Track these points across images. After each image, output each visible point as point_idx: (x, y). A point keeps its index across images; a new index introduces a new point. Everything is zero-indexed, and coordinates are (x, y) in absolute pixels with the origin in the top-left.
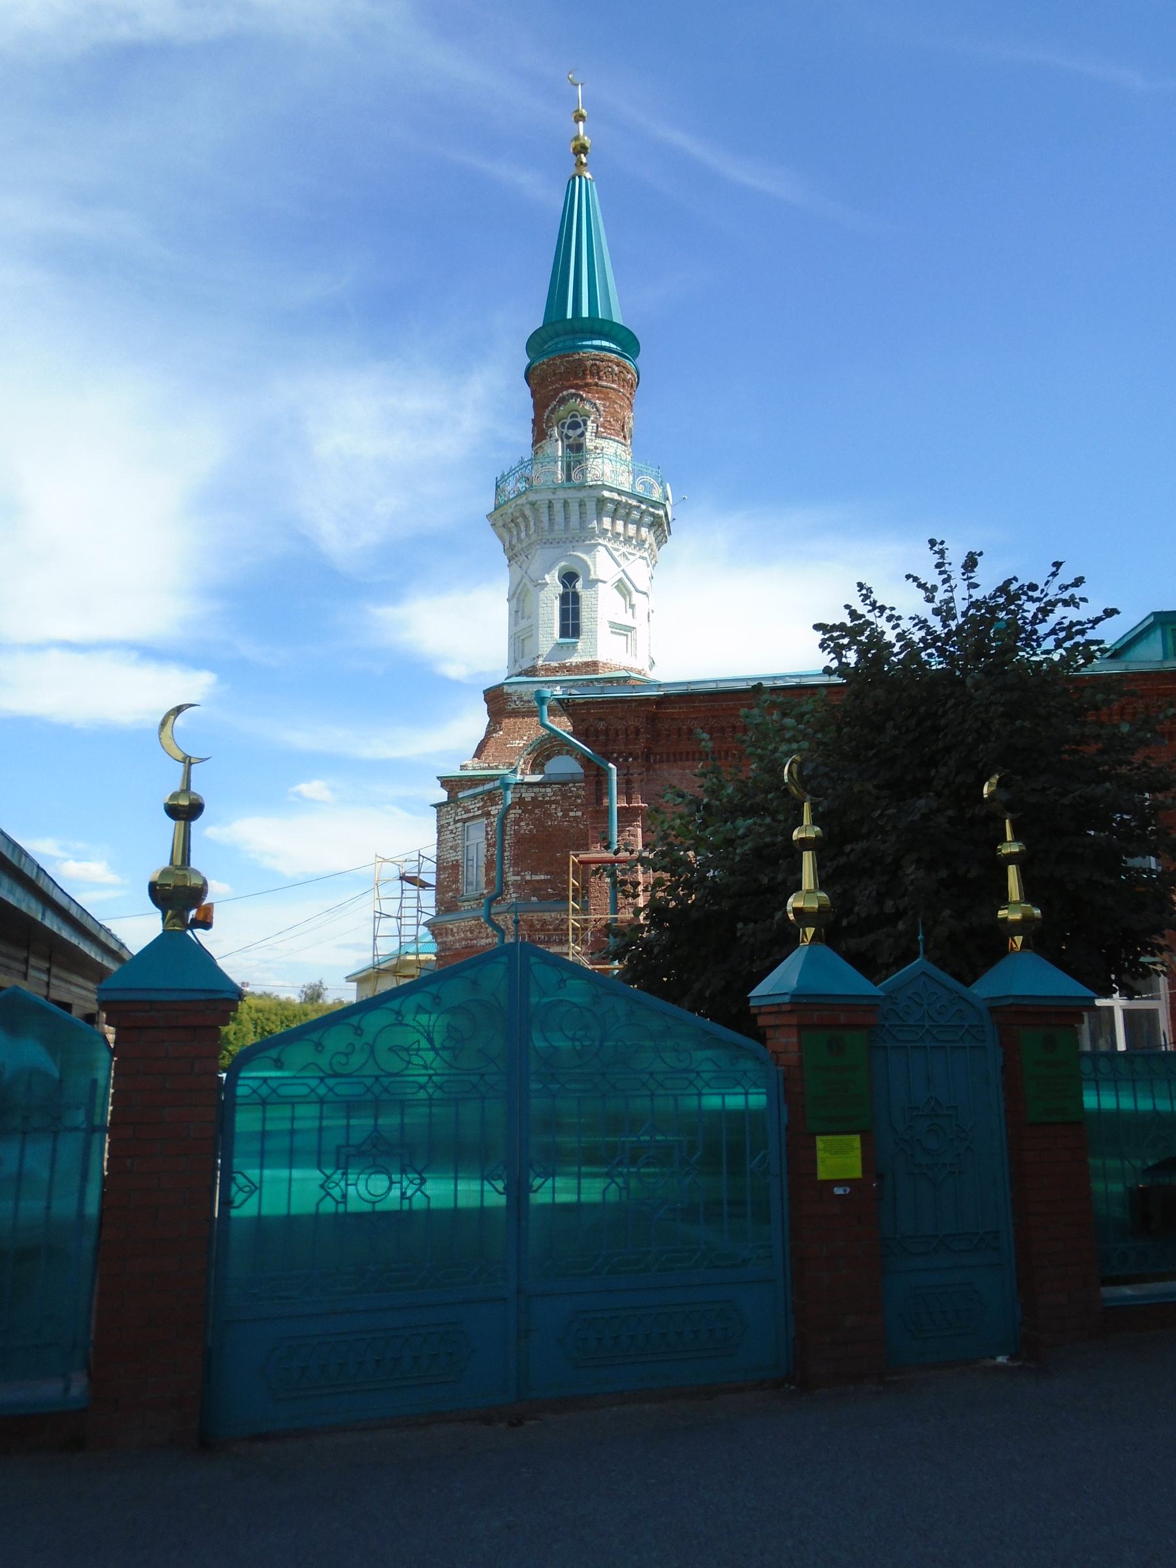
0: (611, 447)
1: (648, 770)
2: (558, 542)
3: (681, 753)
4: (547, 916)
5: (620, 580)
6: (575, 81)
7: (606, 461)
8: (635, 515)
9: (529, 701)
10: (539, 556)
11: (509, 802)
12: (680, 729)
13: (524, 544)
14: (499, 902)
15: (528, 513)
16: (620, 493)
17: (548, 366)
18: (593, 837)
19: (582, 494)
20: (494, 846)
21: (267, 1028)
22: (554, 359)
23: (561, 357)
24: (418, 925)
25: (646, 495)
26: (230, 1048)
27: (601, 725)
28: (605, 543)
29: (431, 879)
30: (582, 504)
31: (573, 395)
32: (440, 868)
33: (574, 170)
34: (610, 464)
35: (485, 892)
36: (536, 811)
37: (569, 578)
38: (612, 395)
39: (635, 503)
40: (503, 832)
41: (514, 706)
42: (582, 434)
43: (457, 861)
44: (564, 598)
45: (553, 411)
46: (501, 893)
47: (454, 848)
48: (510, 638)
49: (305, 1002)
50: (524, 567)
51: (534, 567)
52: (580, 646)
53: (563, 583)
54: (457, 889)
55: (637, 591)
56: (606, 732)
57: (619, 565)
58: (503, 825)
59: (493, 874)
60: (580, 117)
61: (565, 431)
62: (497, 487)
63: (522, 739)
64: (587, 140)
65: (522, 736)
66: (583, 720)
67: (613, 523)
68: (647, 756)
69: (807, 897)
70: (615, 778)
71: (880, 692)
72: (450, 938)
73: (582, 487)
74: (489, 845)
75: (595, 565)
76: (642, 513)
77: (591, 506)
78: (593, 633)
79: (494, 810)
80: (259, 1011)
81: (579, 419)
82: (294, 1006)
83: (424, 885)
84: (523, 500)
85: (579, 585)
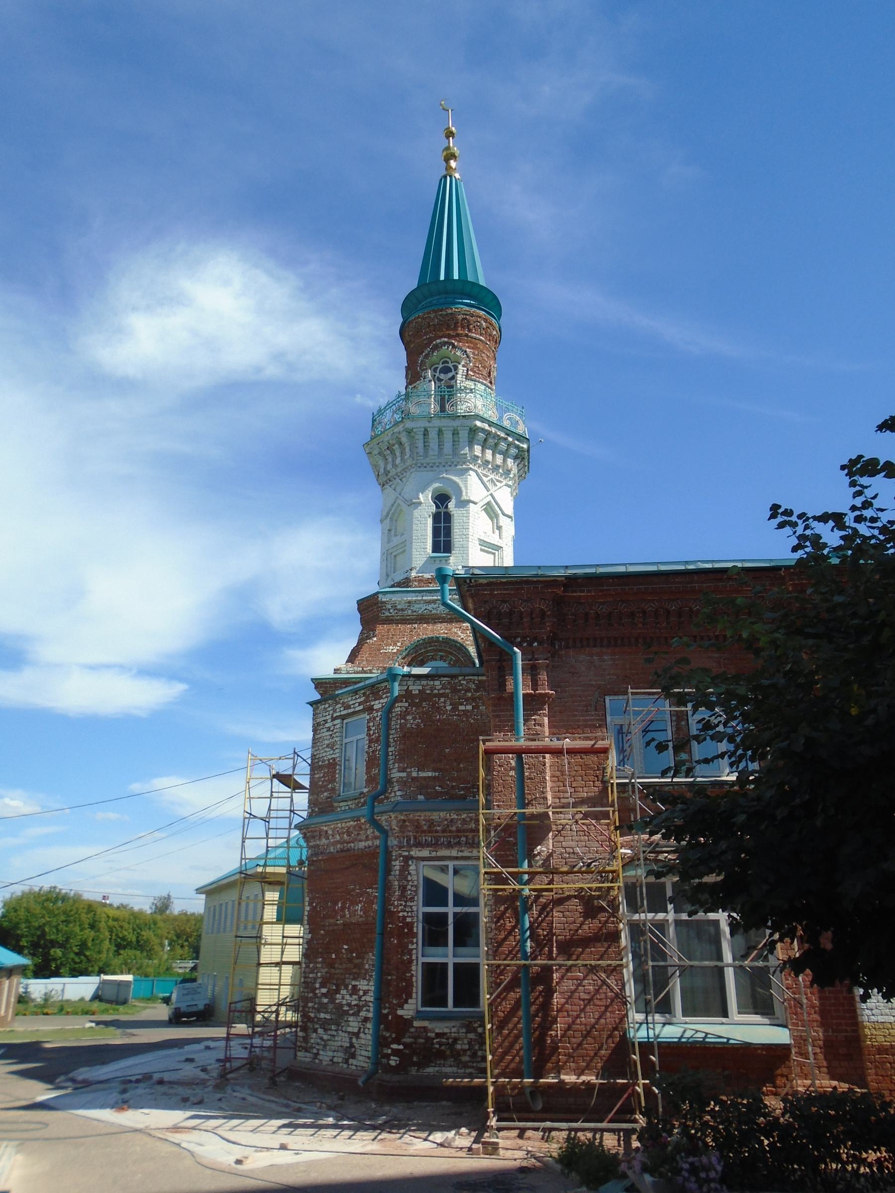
1: (553, 656)
2: (432, 466)
3: (588, 639)
4: (435, 816)
5: (488, 504)
6: (446, 108)
7: (478, 396)
8: (503, 446)
9: (402, 610)
10: (414, 478)
11: (396, 694)
12: (587, 614)
13: (399, 470)
14: (381, 802)
15: (404, 439)
16: (491, 424)
18: (495, 726)
19: (456, 423)
20: (377, 741)
21: (121, 935)
22: (428, 313)
23: (435, 311)
24: (290, 828)
26: (88, 953)
27: (505, 607)
29: (305, 782)
30: (455, 433)
31: (445, 343)
32: (315, 767)
33: (444, 173)
35: (365, 790)
36: (424, 704)
37: (441, 499)
38: (480, 346)
40: (388, 727)
41: (387, 614)
42: (453, 378)
43: (334, 759)
44: (436, 518)
45: (427, 356)
46: (384, 791)
47: (331, 746)
48: (383, 554)
49: (155, 912)
50: (398, 489)
51: (408, 488)
53: (435, 503)
54: (333, 789)
55: (504, 514)
56: (511, 613)
57: (488, 490)
58: (388, 720)
59: (375, 771)
60: (449, 134)
61: (437, 374)
62: (374, 421)
63: (395, 645)
65: (393, 645)
66: (486, 602)
67: (483, 451)
68: (553, 639)
70: (520, 662)
72: (324, 841)
73: (455, 417)
74: (371, 741)
75: (466, 487)
76: (509, 445)
77: (464, 435)
79: (377, 705)
80: (115, 920)
81: (450, 365)
82: (146, 915)
83: (297, 786)
84: (400, 427)
85: (451, 505)
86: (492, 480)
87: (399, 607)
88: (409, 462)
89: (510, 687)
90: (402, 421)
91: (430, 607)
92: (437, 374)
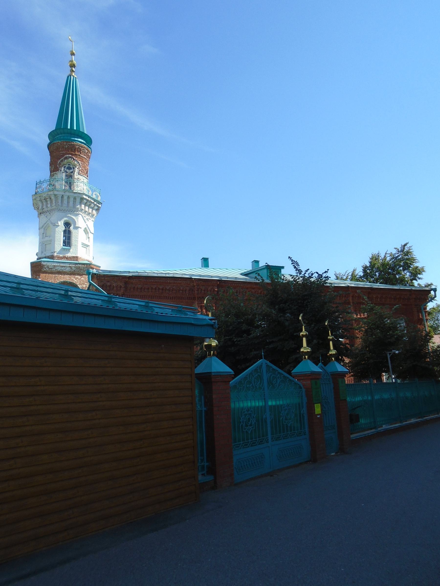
0: (83, 178)
8: (92, 205)
9: (51, 269)
15: (53, 198)
16: (89, 197)
17: (61, 144)
19: (75, 195)
22: (63, 142)
25: (96, 199)
27: (109, 284)
28: (82, 214)
30: (75, 199)
31: (70, 157)
34: (82, 185)
37: (67, 224)
39: (93, 201)
44: (65, 232)
45: (62, 161)
52: (71, 250)
57: (86, 222)
64: (75, 62)
67: (85, 207)
69: (305, 348)
71: (286, 295)
76: (95, 205)
77: (78, 200)
78: (76, 246)
81: (71, 166)
84: (52, 193)
85: (71, 228)
86: (87, 219)
87: (50, 267)
88: (54, 207)
89: (421, 317)
90: (53, 191)
91: (63, 268)
92: (66, 169)
